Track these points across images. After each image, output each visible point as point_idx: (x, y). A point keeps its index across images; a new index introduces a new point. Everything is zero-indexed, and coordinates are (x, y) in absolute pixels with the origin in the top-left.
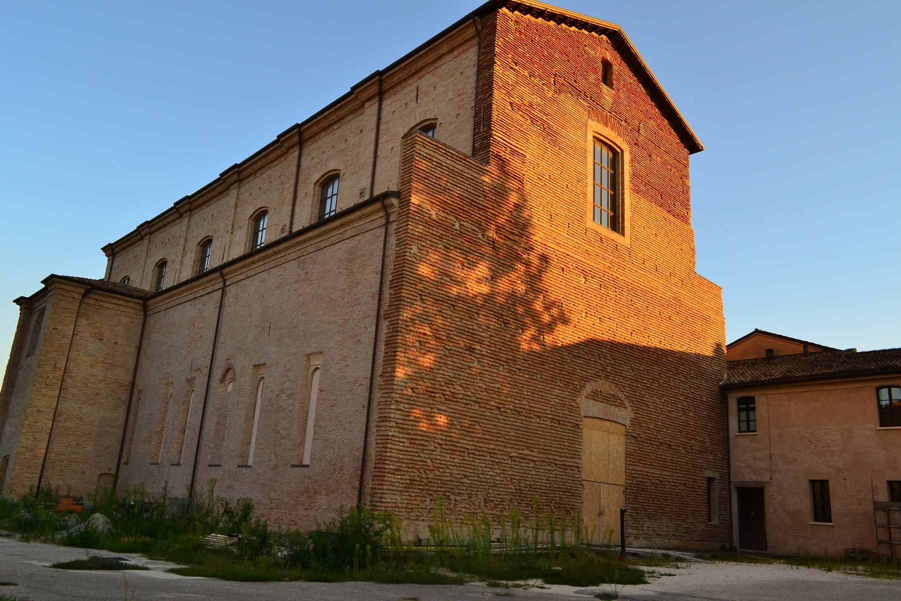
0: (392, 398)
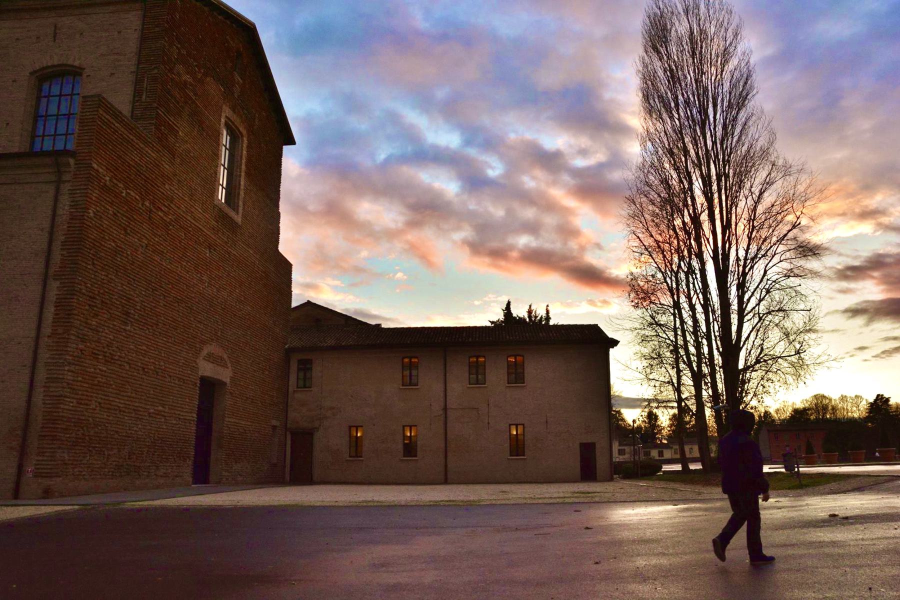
0: (65, 359)
